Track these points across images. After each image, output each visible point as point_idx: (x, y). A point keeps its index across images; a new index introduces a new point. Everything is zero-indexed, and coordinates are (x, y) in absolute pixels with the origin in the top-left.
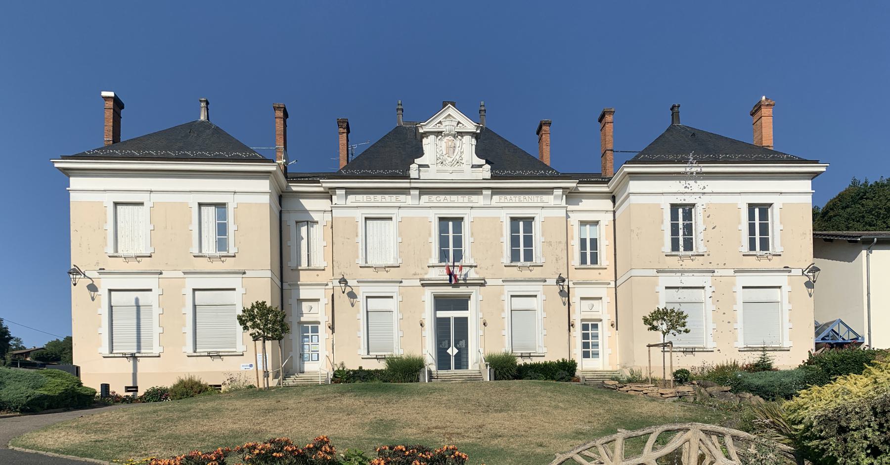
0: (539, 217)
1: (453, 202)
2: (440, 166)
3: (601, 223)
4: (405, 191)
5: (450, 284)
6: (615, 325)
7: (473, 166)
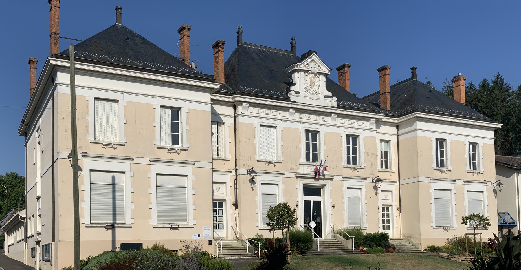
1: (313, 119)
2: (306, 94)
4: (286, 109)
5: (315, 179)
6: (399, 209)
7: (326, 97)
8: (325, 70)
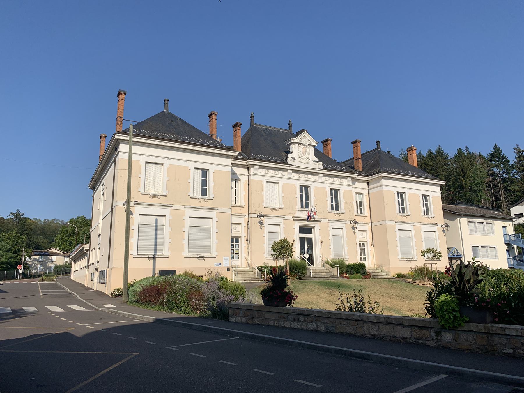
0: (342, 189)
1: (305, 178)
3: (280, 183)
4: (285, 170)
5: (307, 221)
7: (314, 161)
8: (314, 143)
